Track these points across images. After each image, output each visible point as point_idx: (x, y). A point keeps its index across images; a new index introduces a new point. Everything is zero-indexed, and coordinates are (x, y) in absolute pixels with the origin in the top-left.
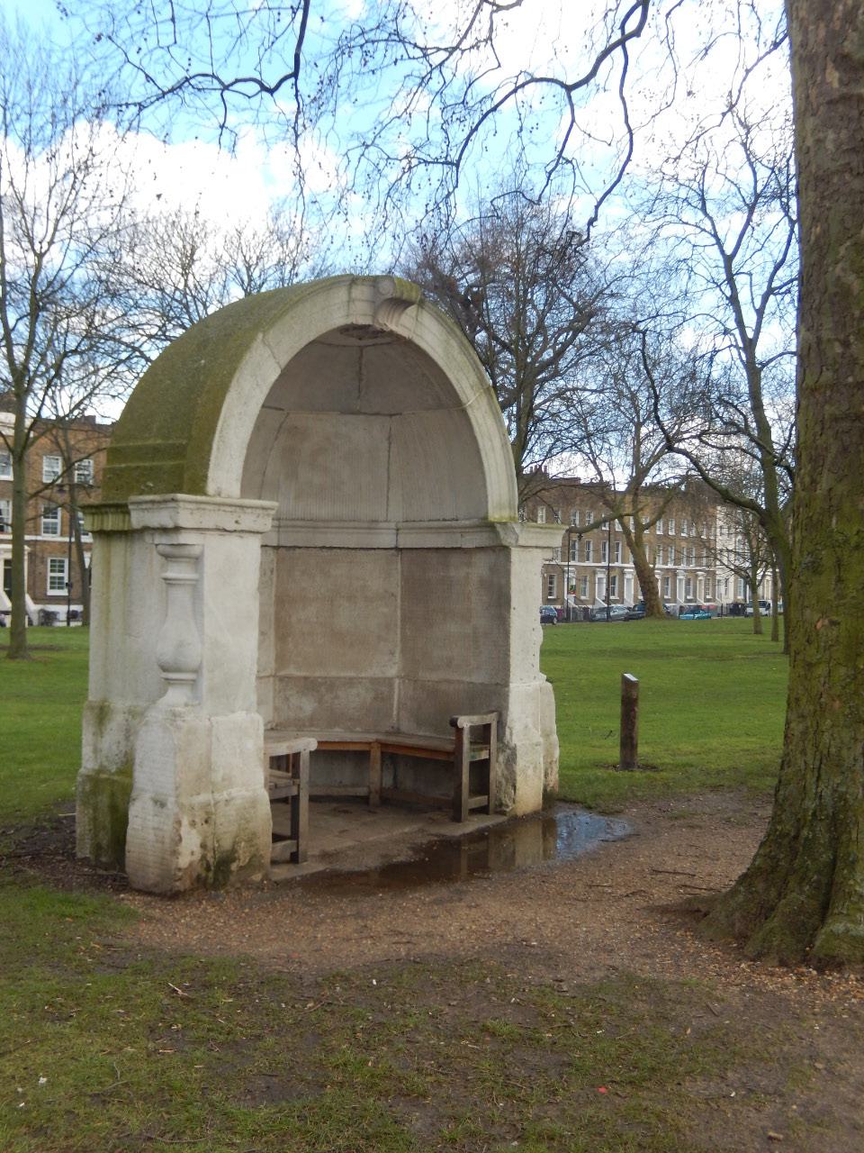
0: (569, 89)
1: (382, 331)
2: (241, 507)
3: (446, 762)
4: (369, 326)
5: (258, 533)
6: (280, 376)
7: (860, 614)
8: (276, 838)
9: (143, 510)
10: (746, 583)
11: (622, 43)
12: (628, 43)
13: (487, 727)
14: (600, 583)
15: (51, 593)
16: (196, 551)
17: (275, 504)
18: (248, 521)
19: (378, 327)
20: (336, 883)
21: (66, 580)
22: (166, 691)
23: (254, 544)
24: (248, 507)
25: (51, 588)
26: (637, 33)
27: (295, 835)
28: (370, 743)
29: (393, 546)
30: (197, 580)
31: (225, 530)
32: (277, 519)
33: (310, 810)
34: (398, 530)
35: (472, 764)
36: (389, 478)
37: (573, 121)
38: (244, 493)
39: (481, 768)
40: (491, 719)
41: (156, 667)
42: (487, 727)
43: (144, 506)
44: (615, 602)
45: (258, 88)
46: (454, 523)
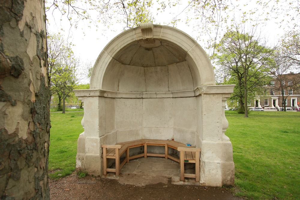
29: (194, 96)
36: (192, 77)
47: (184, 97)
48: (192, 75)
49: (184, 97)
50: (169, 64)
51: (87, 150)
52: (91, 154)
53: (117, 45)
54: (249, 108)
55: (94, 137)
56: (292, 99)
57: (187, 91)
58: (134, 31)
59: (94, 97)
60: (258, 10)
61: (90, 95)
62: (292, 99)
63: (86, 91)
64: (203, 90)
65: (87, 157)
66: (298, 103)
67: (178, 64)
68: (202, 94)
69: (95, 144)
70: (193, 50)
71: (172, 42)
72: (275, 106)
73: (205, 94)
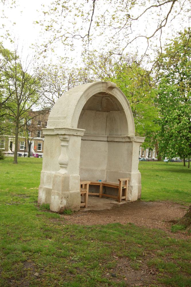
0: (148, 38)
1: (108, 94)
2: (78, 130)
3: (116, 189)
4: (105, 92)
5: (81, 136)
6: (86, 102)
7: (53, 104)
8: (82, 202)
9: (57, 130)
10: (11, 78)
11: (161, 28)
12: (162, 28)
13: (126, 181)
14: (147, 152)
15: (21, 149)
16: (68, 139)
17: (85, 130)
18: (79, 134)
19: (107, 93)
20: (93, 212)
21: (24, 147)
22: (60, 169)
23: (80, 138)
24: (79, 131)
25: (21, 148)
26: (164, 26)
27: (85, 202)
28: (100, 184)
29: (106, 140)
30: (68, 146)
31: (74, 135)
32: (145, 140)
33: (88, 198)
34: (108, 137)
35: (123, 189)
36: (106, 126)
37: (148, 46)
38: (78, 128)
39: (124, 190)
40: (127, 179)
41: (59, 164)
42: (126, 181)
43: (57, 129)
44: (150, 157)
45: (80, 37)
46: (120, 136)
47: (95, 141)
48: (106, 124)
49: (95, 141)
50: (88, 110)
51: (70, 188)
52: (73, 191)
53: (91, 91)
54: (3, 152)
55: (77, 175)
56: (10, 141)
57: (97, 135)
58: (102, 84)
59: (78, 136)
60: (74, 50)
61: (77, 135)
62: (10, 141)
63: (76, 130)
64: (134, 139)
65: (71, 194)
66: (34, 147)
67: (98, 112)
68: (133, 142)
69: (77, 181)
70: (127, 110)
71: (118, 100)
72: (11, 150)
73: (135, 142)
